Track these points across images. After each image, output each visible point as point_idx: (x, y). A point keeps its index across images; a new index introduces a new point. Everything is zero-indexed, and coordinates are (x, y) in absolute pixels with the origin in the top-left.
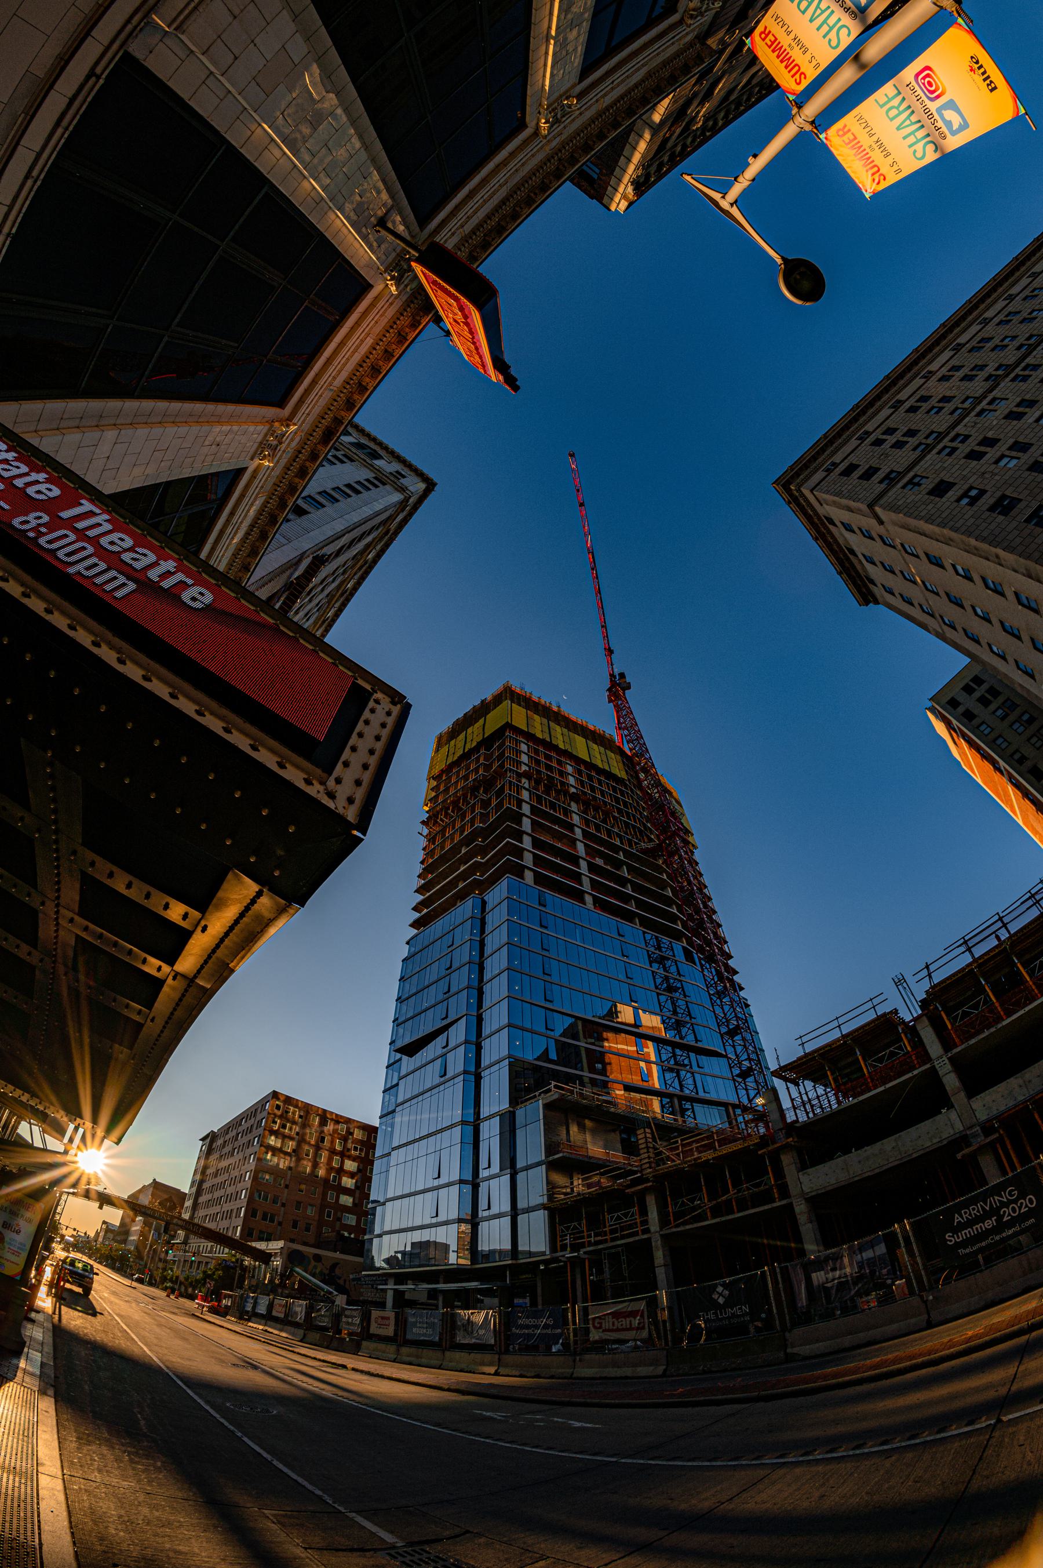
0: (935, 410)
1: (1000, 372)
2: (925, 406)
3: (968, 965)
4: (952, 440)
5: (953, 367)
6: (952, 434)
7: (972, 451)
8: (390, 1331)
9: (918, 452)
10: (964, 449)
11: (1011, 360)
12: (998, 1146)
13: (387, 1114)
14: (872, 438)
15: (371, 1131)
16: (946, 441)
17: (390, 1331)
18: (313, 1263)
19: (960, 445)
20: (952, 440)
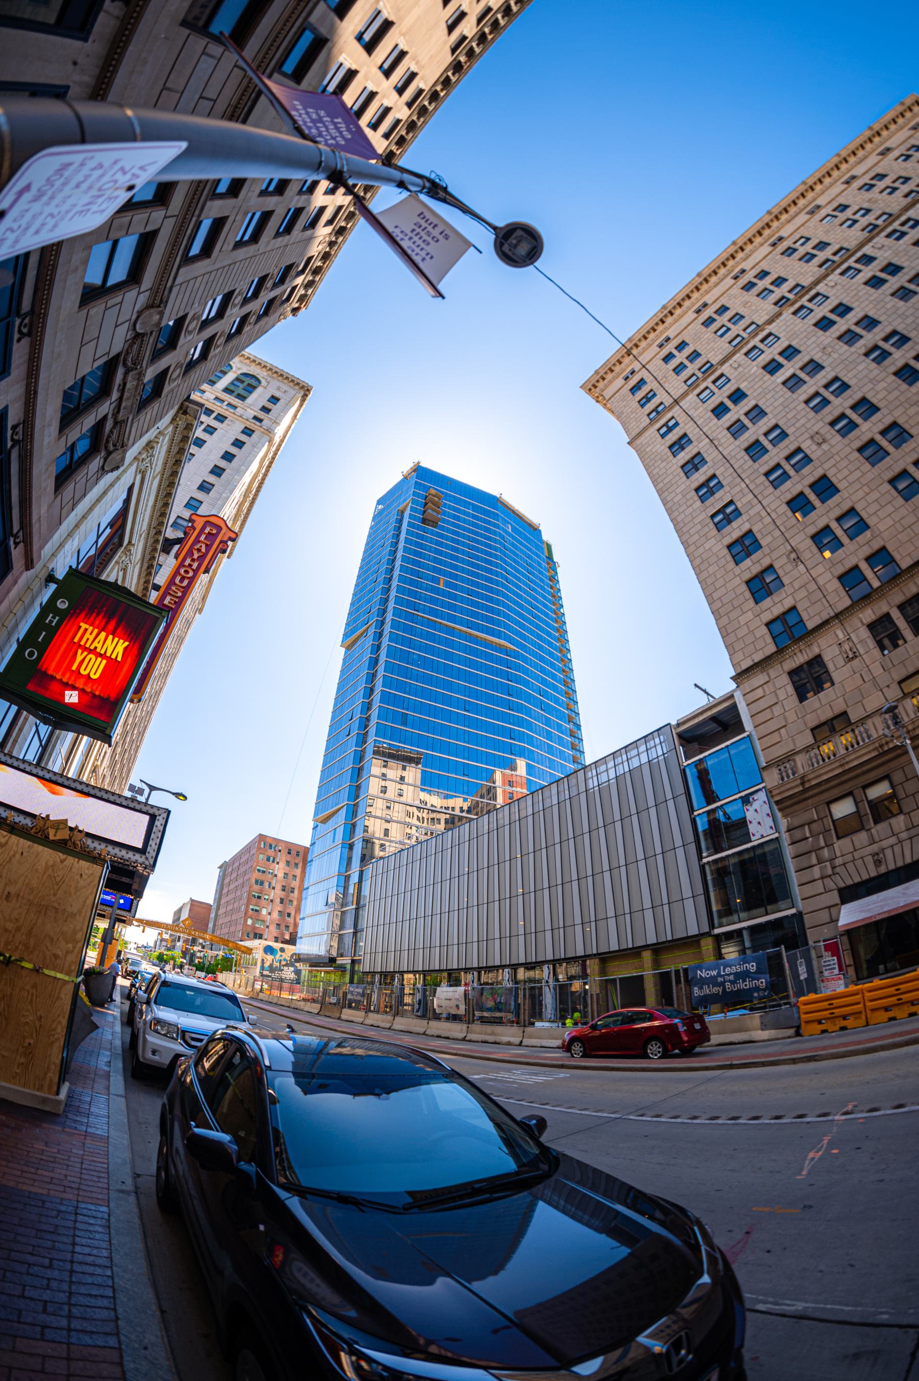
0: (849, 223)
1: (836, 258)
2: (881, 185)
3: (549, 1203)
4: (903, 224)
5: (877, 175)
6: (903, 218)
7: (874, 277)
8: (406, 976)
9: (909, 199)
10: (868, 272)
11: (894, 208)
12: (696, 1228)
13: (313, 844)
14: (823, 213)
15: (306, 850)
16: (896, 225)
17: (406, 976)
18: (279, 953)
19: (909, 230)
20: (903, 224)
